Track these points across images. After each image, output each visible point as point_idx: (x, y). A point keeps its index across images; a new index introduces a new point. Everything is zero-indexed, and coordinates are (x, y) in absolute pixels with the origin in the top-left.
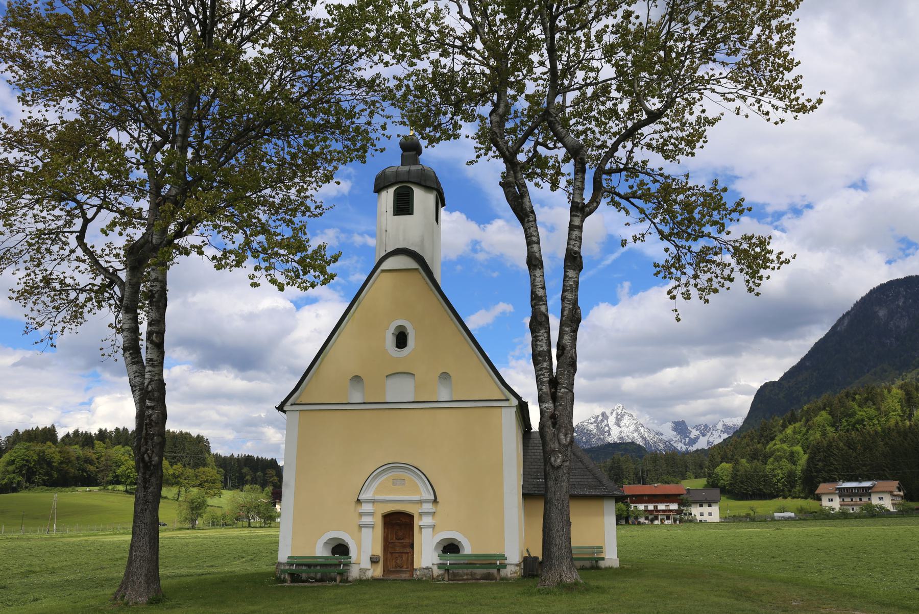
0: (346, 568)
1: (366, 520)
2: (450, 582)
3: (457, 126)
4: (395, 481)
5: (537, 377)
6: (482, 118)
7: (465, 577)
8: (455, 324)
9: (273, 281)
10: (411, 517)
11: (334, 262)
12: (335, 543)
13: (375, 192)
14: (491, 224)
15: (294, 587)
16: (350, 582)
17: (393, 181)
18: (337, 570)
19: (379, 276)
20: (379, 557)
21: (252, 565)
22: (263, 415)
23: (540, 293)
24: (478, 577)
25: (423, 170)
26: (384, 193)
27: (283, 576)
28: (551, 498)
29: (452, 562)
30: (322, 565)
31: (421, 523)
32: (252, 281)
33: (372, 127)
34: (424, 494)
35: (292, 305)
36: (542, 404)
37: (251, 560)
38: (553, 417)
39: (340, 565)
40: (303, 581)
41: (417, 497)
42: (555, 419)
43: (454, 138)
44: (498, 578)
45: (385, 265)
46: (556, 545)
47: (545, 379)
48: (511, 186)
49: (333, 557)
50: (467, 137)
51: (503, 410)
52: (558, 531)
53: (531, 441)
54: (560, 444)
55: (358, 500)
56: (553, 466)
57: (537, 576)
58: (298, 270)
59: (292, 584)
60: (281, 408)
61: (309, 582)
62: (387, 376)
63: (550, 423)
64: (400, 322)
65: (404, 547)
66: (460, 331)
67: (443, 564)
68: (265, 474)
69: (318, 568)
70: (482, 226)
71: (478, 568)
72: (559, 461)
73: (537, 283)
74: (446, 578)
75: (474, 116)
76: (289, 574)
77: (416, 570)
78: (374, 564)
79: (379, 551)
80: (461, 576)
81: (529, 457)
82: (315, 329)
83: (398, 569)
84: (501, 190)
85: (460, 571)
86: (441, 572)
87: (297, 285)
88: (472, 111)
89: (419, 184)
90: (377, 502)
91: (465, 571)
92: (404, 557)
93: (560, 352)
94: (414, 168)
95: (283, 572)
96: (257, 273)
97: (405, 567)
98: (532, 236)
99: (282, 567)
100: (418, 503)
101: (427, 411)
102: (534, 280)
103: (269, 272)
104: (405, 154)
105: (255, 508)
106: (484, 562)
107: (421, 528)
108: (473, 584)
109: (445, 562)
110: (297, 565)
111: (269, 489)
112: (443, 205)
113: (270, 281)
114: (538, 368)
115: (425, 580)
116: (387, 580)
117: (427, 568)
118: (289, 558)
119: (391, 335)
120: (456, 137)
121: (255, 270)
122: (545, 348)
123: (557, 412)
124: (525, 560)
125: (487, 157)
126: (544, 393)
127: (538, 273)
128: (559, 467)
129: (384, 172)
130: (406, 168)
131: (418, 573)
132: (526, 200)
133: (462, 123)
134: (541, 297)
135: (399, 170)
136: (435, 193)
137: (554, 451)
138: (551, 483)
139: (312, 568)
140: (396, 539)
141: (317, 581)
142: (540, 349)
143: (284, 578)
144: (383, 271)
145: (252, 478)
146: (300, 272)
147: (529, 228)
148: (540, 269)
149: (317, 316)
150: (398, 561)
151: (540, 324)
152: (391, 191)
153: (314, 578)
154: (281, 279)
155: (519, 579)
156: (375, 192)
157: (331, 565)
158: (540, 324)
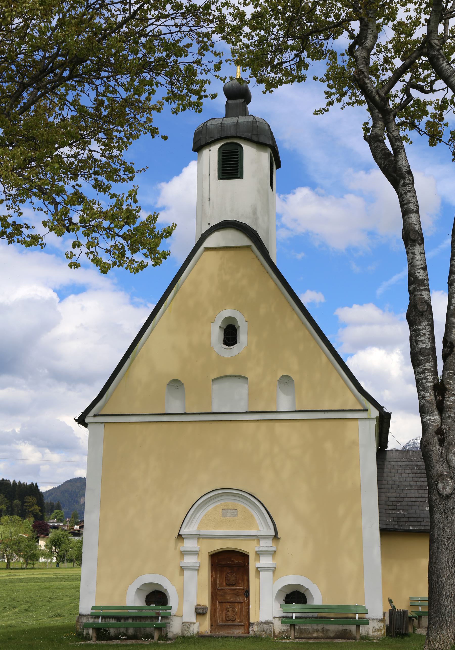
0: (165, 621)
1: (189, 560)
2: (298, 640)
3: (301, 64)
4: (225, 511)
5: (417, 381)
6: (333, 54)
7: (315, 635)
8: (297, 315)
9: (97, 261)
10: (245, 557)
11: (166, 237)
12: (150, 590)
13: (194, 150)
14: (294, 193)
15: (103, 646)
16: (170, 639)
17: (217, 136)
18: (154, 623)
19: (201, 255)
20: (207, 608)
21: (28, 617)
22: (17, 430)
23: (421, 275)
24: (332, 635)
25: (255, 121)
26: (206, 152)
27: (85, 632)
28: (439, 536)
29: (298, 615)
30: (134, 618)
31: (258, 565)
32: (70, 261)
33: (203, 67)
34: (261, 529)
35: (55, 295)
36: (424, 415)
37: (26, 610)
38: (440, 432)
39: (157, 618)
40: (111, 638)
41: (253, 532)
42: (442, 434)
43: (299, 81)
44: (358, 637)
45: (210, 242)
46: (447, 596)
47: (429, 384)
48: (379, 141)
49: (148, 607)
50: (315, 79)
51: (360, 423)
52: (449, 579)
53: (387, 463)
54: (449, 466)
55: (179, 535)
56: (440, 495)
57: (407, 635)
58: (123, 248)
59: (99, 642)
60: (81, 420)
61: (119, 639)
62: (213, 381)
63: (436, 439)
64: (227, 313)
65: (237, 594)
66: (303, 323)
67: (286, 617)
68: (23, 502)
69: (130, 621)
70: (282, 196)
71: (332, 623)
72: (448, 488)
73: (417, 263)
74: (292, 637)
75: (323, 52)
76: (94, 628)
77: (253, 624)
78: (200, 617)
79: (205, 601)
80: (310, 633)
81: (384, 482)
82: (82, 325)
83: (230, 623)
84: (366, 145)
85: (309, 627)
86: (285, 628)
87: (125, 266)
88: (322, 45)
89: (249, 140)
90: (203, 538)
91: (315, 627)
92: (237, 608)
93: (448, 350)
94: (242, 119)
95: (87, 626)
96: (76, 251)
97: (238, 620)
98: (409, 203)
99: (85, 620)
100: (254, 539)
101: (175, 425)
102: (413, 259)
103: (91, 250)
104: (230, 102)
105: (15, 544)
106: (339, 616)
107: (258, 571)
108: (327, 643)
109: (290, 615)
110: (103, 617)
111: (29, 521)
112: (278, 166)
113: (92, 261)
114: (418, 370)
115: (266, 638)
116: (217, 637)
117: (267, 623)
118: (93, 608)
119: (218, 328)
120: (301, 79)
121: (74, 247)
122: (428, 345)
123: (444, 427)
124: (392, 612)
125: (340, 105)
126: (428, 402)
127: (417, 249)
128: (449, 496)
129: (205, 125)
130: (232, 120)
131: (256, 628)
132: (401, 157)
133: (308, 61)
134: (422, 280)
135: (225, 122)
136: (269, 151)
137: (442, 475)
138: (438, 517)
139: (122, 621)
140: (227, 585)
141: (129, 638)
142: (421, 345)
143: (87, 634)
144: (207, 249)
145: (8, 508)
146: (126, 249)
147: (406, 193)
148: (420, 245)
149: (83, 308)
150: (229, 613)
151: (422, 314)
152: (215, 149)
153: (125, 635)
154: (106, 259)
155: (384, 639)
156: (194, 150)
157: (146, 618)
158: (422, 314)
